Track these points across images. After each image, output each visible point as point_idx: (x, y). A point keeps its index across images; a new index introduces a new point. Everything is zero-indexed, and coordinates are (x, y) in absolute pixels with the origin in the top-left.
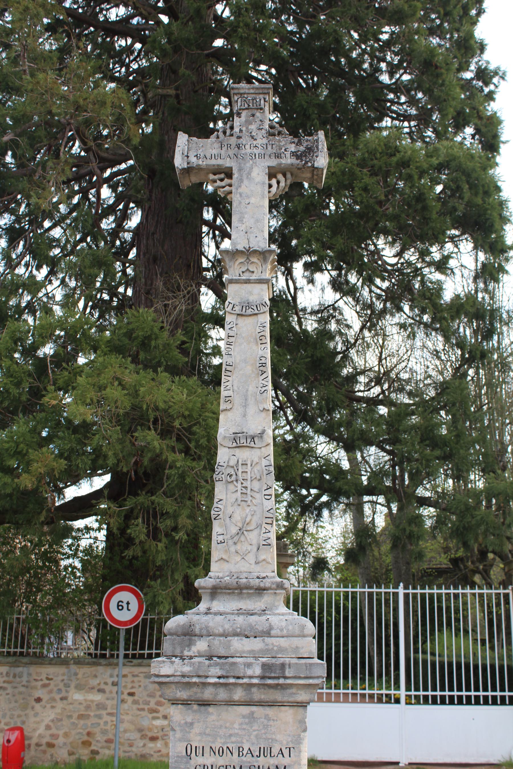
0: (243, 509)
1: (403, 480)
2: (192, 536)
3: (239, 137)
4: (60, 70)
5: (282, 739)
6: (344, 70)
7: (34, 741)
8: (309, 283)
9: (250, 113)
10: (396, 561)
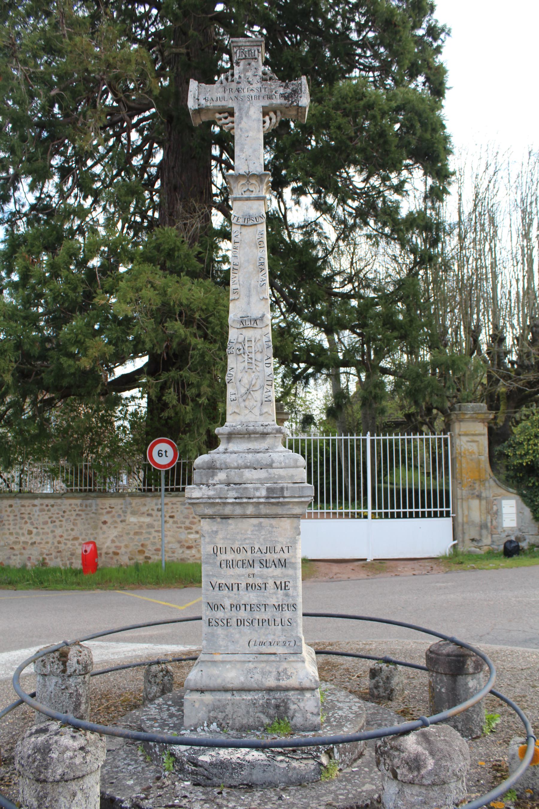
0: (250, 375)
1: (370, 356)
2: (212, 400)
3: (239, 83)
4: (93, 33)
5: (282, 540)
6: (321, 30)
7: (104, 551)
8: (296, 204)
9: (246, 62)
10: (365, 415)
